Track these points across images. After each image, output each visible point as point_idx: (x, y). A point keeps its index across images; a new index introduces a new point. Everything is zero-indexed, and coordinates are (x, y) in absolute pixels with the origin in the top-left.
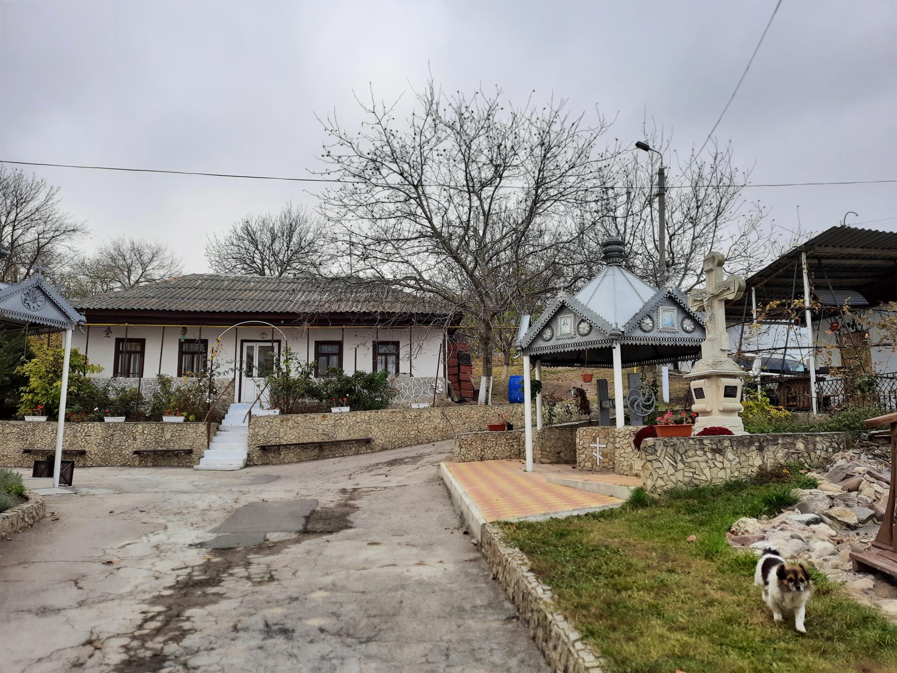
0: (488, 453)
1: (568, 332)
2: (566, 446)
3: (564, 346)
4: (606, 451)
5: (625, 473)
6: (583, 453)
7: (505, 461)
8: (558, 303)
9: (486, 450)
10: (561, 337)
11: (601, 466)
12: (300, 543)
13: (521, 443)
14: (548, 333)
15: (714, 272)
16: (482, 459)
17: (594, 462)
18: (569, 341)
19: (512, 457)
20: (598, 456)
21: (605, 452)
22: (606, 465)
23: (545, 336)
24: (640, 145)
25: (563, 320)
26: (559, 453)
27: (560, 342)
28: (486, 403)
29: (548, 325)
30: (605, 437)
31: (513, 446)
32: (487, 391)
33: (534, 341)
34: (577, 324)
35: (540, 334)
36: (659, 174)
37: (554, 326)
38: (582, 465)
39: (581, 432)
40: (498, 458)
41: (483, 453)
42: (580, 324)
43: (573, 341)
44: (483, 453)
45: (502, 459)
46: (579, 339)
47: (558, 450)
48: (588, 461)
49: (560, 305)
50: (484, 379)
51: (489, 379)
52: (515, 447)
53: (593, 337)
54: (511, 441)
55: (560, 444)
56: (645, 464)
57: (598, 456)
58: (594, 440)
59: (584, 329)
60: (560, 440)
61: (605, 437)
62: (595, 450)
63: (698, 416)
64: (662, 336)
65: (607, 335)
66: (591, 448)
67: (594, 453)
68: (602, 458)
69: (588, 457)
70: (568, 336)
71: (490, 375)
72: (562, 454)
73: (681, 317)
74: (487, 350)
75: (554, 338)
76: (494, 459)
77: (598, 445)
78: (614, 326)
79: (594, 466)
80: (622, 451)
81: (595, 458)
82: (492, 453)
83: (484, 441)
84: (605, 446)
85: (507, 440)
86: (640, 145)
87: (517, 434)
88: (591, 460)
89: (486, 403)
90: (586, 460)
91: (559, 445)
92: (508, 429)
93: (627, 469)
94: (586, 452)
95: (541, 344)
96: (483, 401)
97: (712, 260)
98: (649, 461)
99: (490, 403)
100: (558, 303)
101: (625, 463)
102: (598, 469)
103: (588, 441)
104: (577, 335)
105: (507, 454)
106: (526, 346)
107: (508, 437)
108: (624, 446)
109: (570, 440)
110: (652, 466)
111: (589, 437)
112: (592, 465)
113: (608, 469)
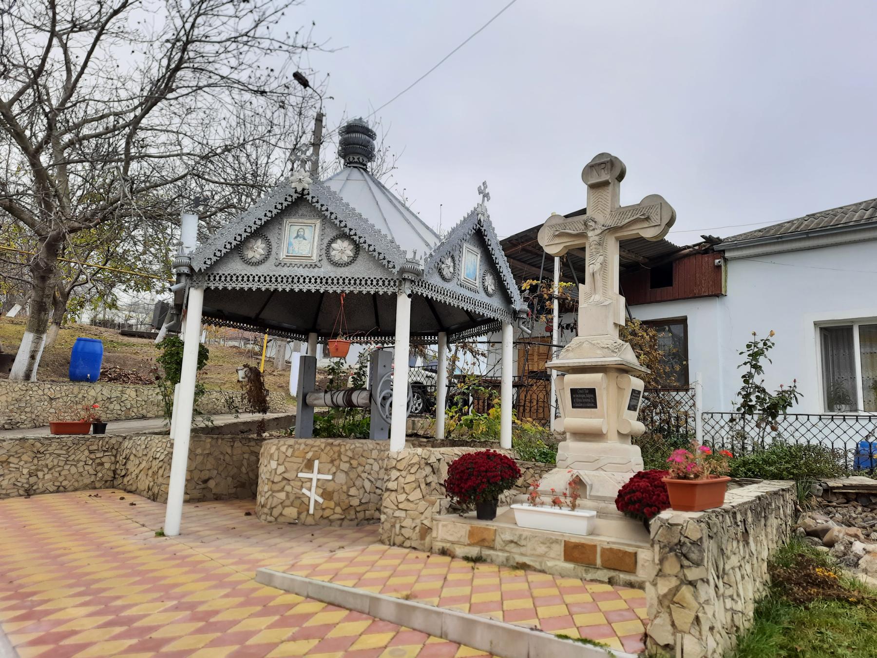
0: (46, 478)
1: (305, 253)
2: (221, 469)
3: (292, 279)
4: (330, 487)
5: (407, 544)
6: (282, 490)
7: (84, 495)
8: (292, 192)
9: (40, 474)
10: (288, 261)
11: (318, 516)
12: (307, 81)
13: (120, 458)
14: (258, 249)
15: (611, 187)
16: (29, 493)
17: (301, 503)
18: (305, 272)
19: (98, 485)
20: (313, 496)
21: (330, 489)
22: (327, 513)
23: (250, 254)
24: (297, 76)
25: (295, 228)
26: (205, 481)
27: (285, 271)
28: (27, 377)
29: (260, 232)
30: (332, 461)
31: (102, 464)
32: (33, 357)
33: (222, 260)
34: (326, 241)
35: (238, 249)
36: (316, 120)
37: (272, 237)
38: (276, 512)
39: (283, 449)
40: (65, 490)
41: (33, 480)
42: (333, 240)
43: (315, 272)
44: (33, 480)
45: (76, 490)
46: (326, 270)
47: (205, 475)
48: (292, 505)
49: (295, 196)
50: (28, 338)
51: (39, 338)
52: (107, 466)
53: (362, 270)
54: (98, 455)
55: (210, 463)
56: (677, 589)
57: (313, 496)
58: (309, 466)
59: (342, 252)
60: (211, 459)
61: (332, 461)
62: (308, 484)
63: (564, 439)
64: (462, 293)
65: (395, 271)
66: (300, 479)
67: (304, 491)
68: (320, 500)
69: (292, 497)
70: (305, 262)
71: (44, 332)
72: (211, 484)
73: (484, 267)
74: (43, 289)
75: (272, 260)
76: (57, 491)
77: (315, 476)
78: (409, 256)
79: (303, 516)
80: (402, 497)
81: (306, 500)
82: (53, 481)
83: (38, 454)
84: (330, 477)
85: (91, 452)
86: (297, 76)
87: (113, 441)
88: (297, 503)
89: (27, 377)
90: (288, 503)
91: (209, 466)
92: (95, 432)
93: (415, 535)
94: (288, 488)
95: (235, 267)
96: (21, 374)
97: (609, 165)
98: (692, 584)
99: (34, 377)
100: (292, 192)
101: (408, 523)
102: (310, 520)
103: (295, 466)
104: (325, 262)
105: (87, 481)
106: (204, 267)
107: (94, 447)
108: (407, 488)
109: (227, 457)
110: (696, 597)
111: (300, 460)
112: (299, 513)
113: (331, 521)
